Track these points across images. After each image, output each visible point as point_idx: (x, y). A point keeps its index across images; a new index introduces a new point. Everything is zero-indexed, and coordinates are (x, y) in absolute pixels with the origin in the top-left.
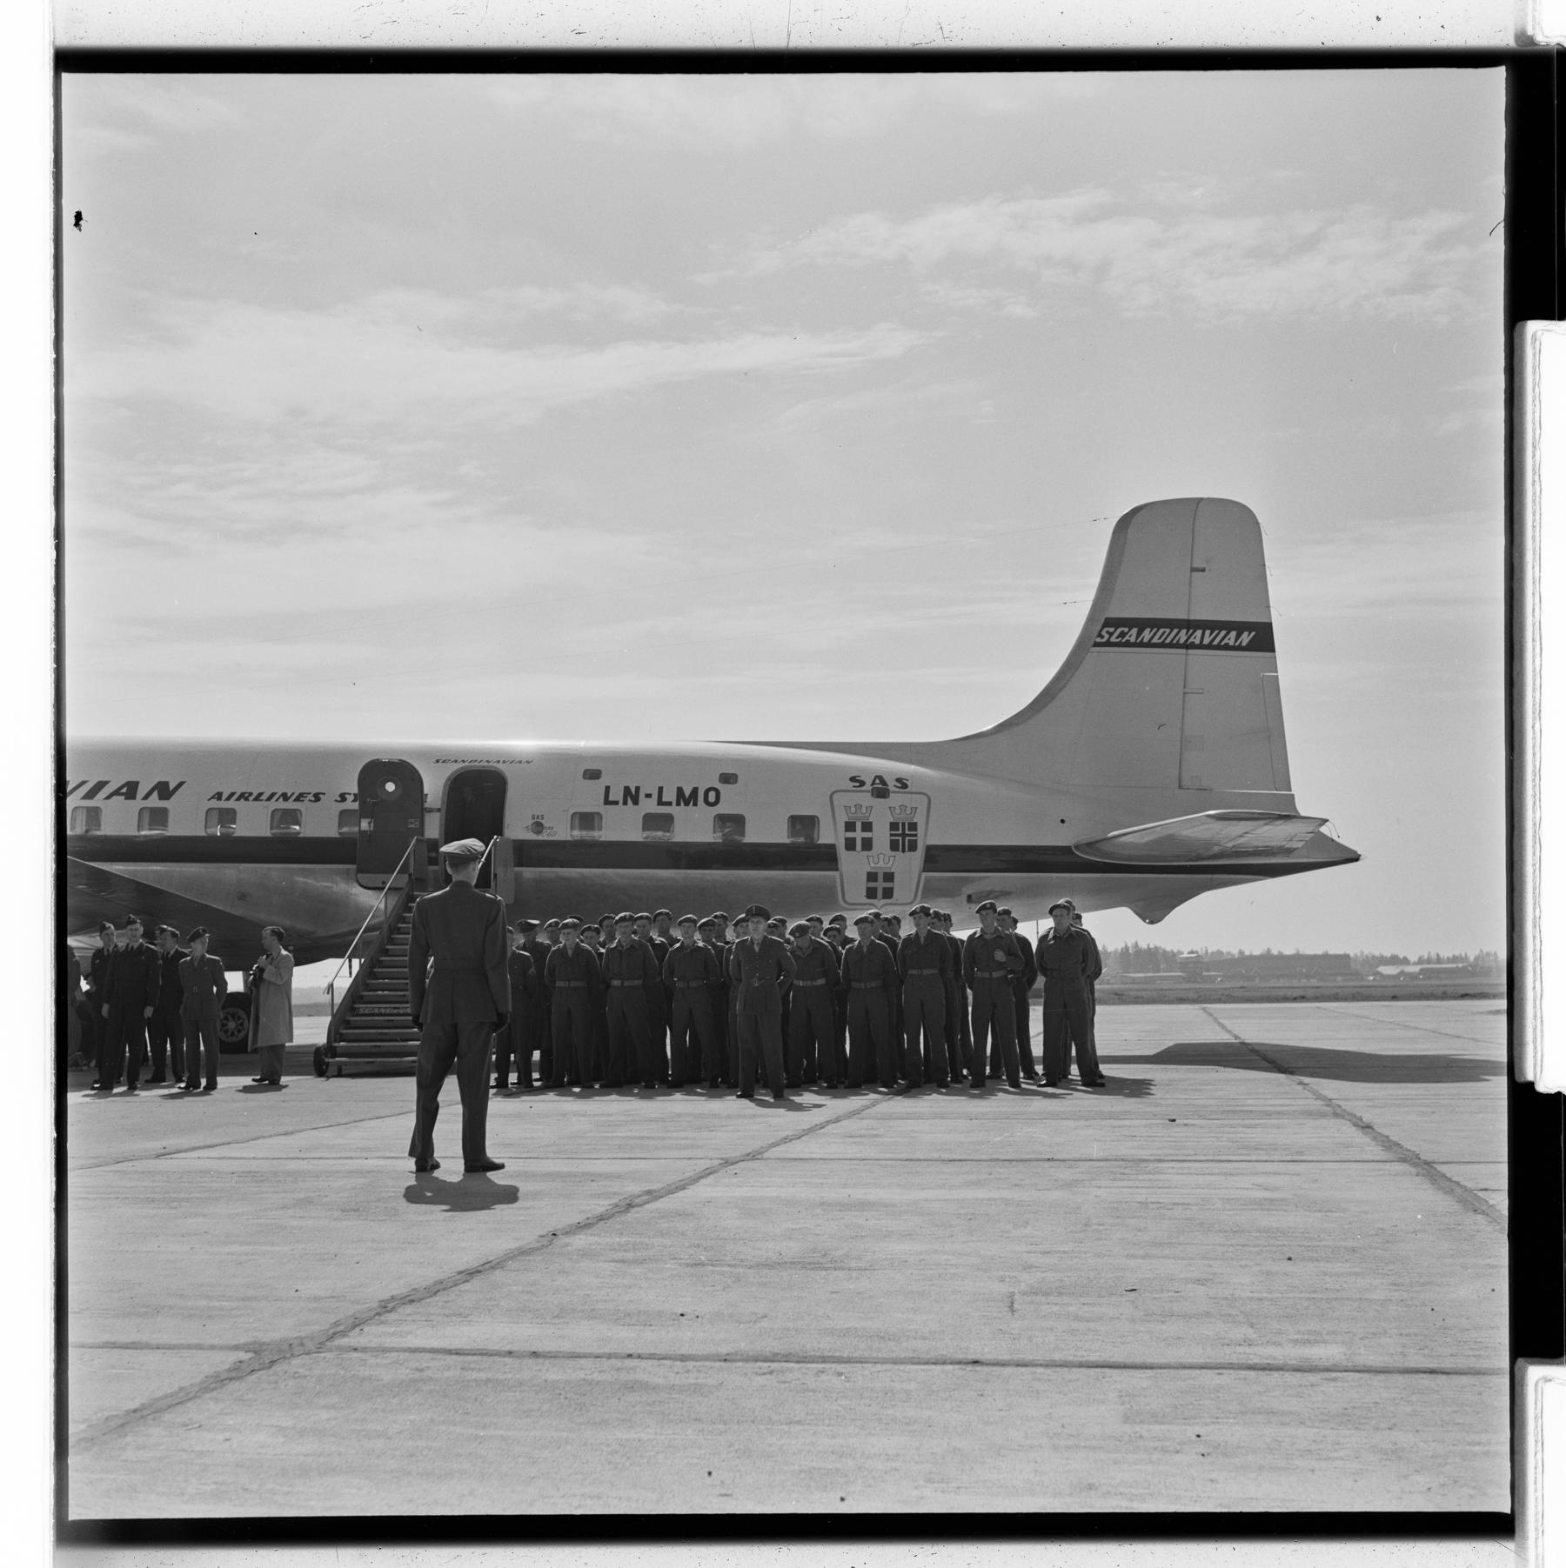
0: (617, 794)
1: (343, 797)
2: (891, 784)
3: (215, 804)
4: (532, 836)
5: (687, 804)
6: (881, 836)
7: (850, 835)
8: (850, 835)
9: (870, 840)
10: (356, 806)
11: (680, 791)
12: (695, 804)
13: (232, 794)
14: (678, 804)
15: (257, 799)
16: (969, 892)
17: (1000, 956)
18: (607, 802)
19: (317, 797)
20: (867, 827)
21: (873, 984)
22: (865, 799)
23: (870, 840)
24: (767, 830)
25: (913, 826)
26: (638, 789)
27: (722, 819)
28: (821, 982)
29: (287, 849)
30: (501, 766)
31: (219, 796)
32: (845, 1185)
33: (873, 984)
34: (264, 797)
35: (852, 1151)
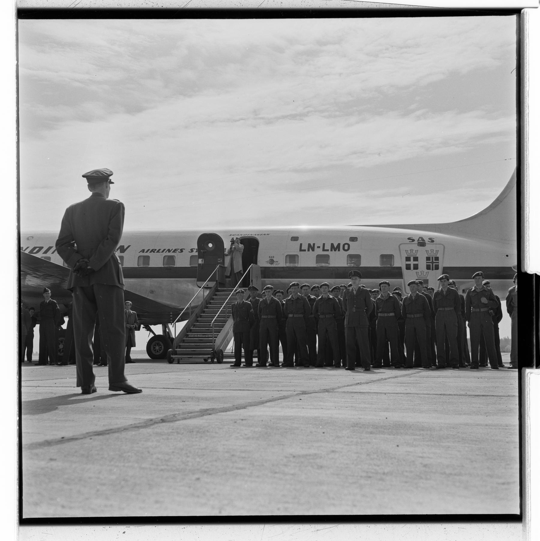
0: (305, 247)
1: (192, 250)
2: (427, 240)
3: (142, 254)
4: (269, 265)
5: (335, 250)
6: (422, 263)
7: (408, 263)
8: (408, 263)
9: (417, 265)
10: (197, 254)
11: (332, 245)
12: (339, 250)
13: (149, 250)
14: (331, 250)
15: (158, 252)
16: (463, 288)
17: (484, 300)
18: (301, 250)
19: (182, 251)
20: (416, 259)
21: (418, 315)
22: (414, 247)
23: (417, 265)
24: (371, 261)
25: (437, 259)
26: (314, 244)
27: (351, 257)
28: (392, 314)
29: (170, 271)
30: (257, 237)
31: (143, 251)
32: (386, 410)
33: (418, 315)
34: (161, 251)
35: (399, 390)
